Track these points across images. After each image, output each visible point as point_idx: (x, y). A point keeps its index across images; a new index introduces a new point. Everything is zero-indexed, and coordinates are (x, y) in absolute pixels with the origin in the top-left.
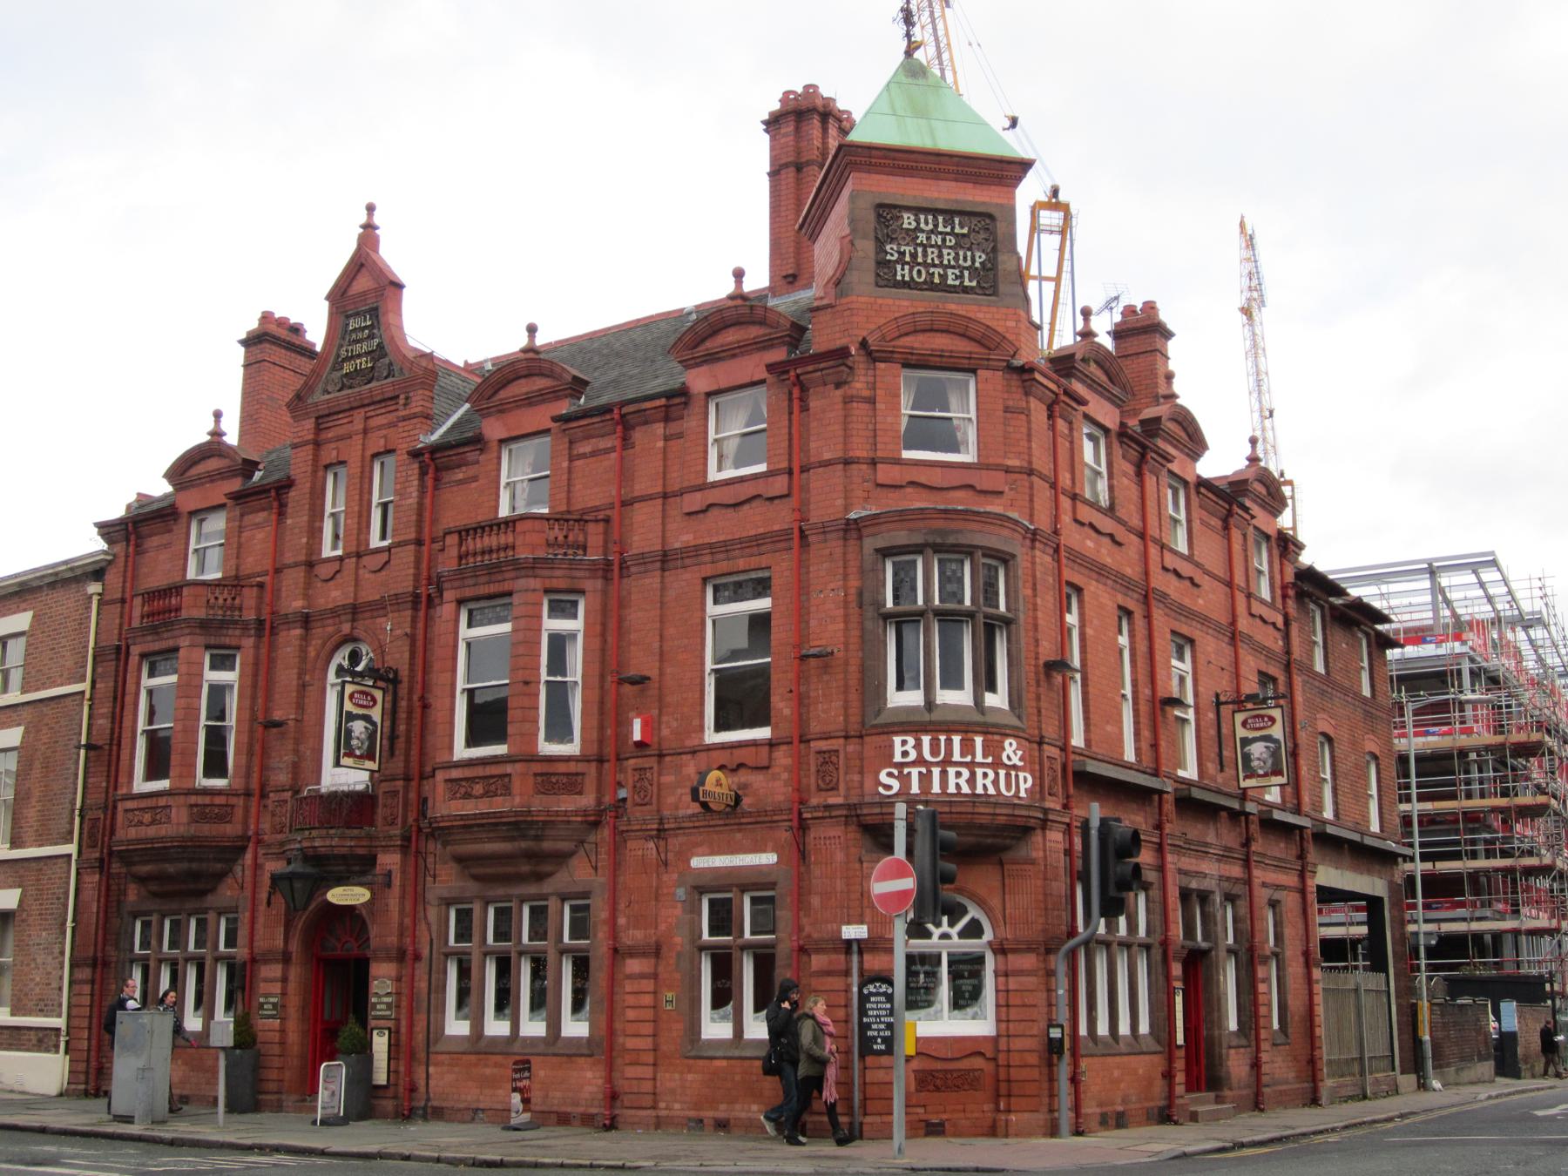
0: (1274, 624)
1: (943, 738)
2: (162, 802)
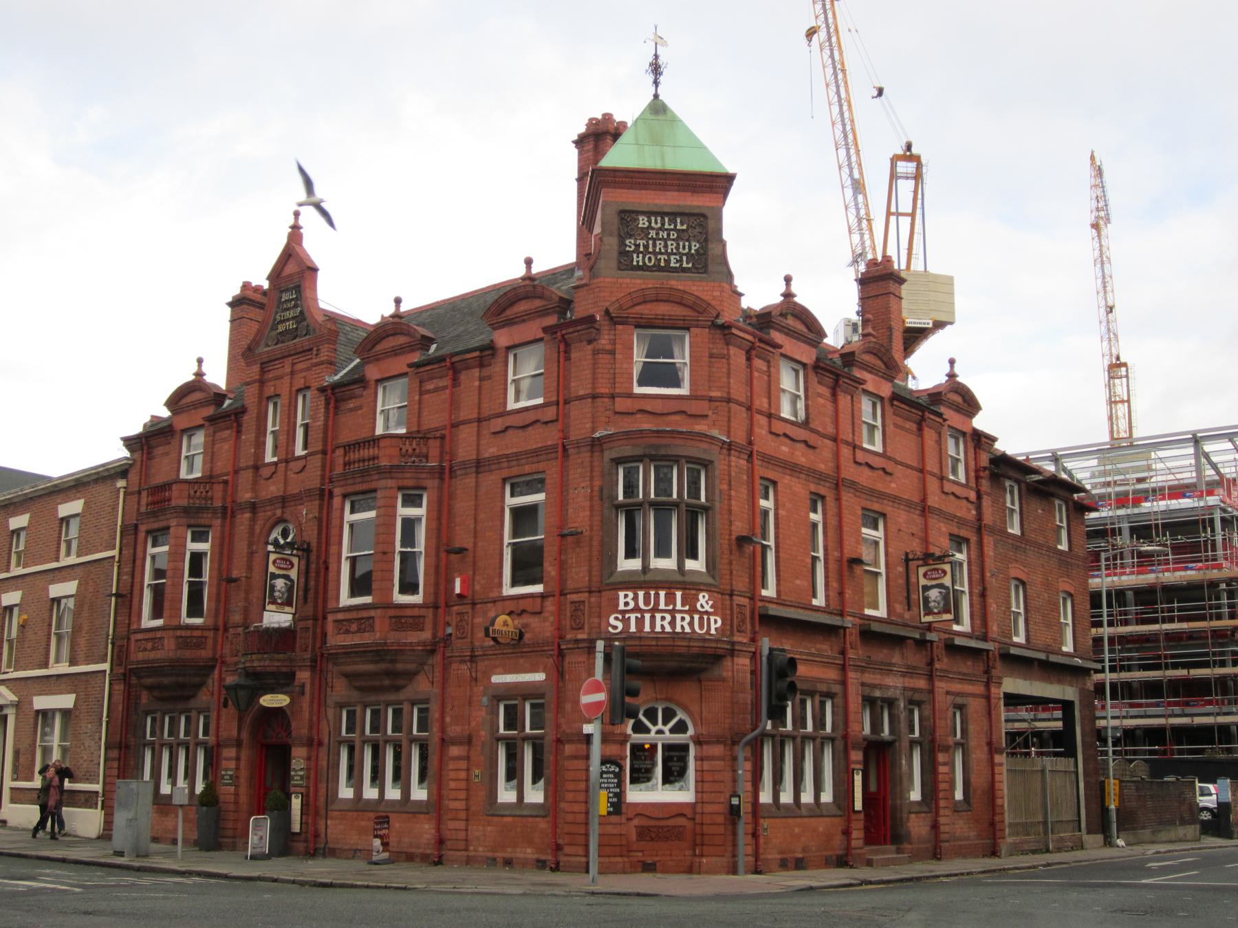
0: (967, 499)
1: (652, 593)
2: (159, 634)
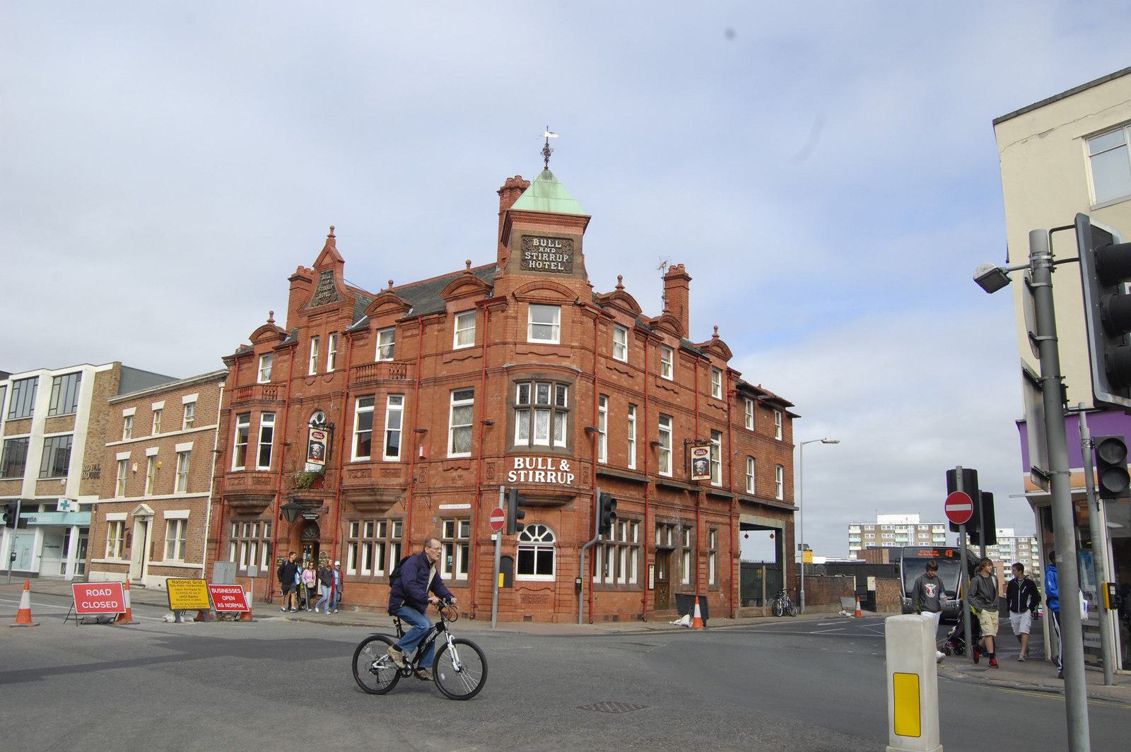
1: (534, 459)
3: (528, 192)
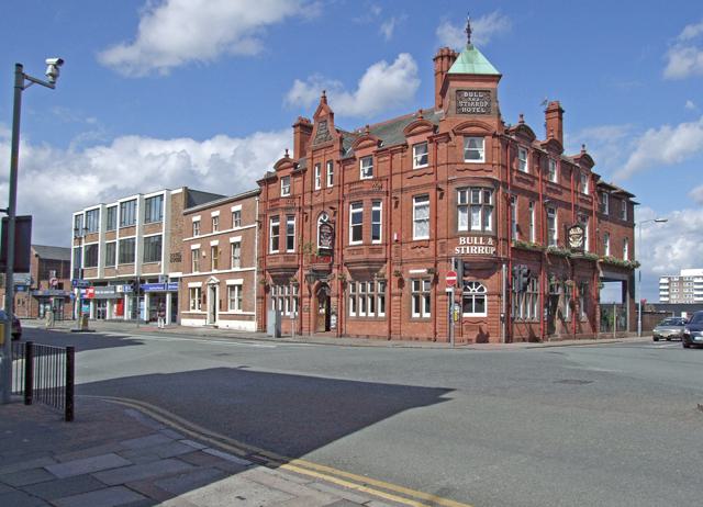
3: (459, 59)
